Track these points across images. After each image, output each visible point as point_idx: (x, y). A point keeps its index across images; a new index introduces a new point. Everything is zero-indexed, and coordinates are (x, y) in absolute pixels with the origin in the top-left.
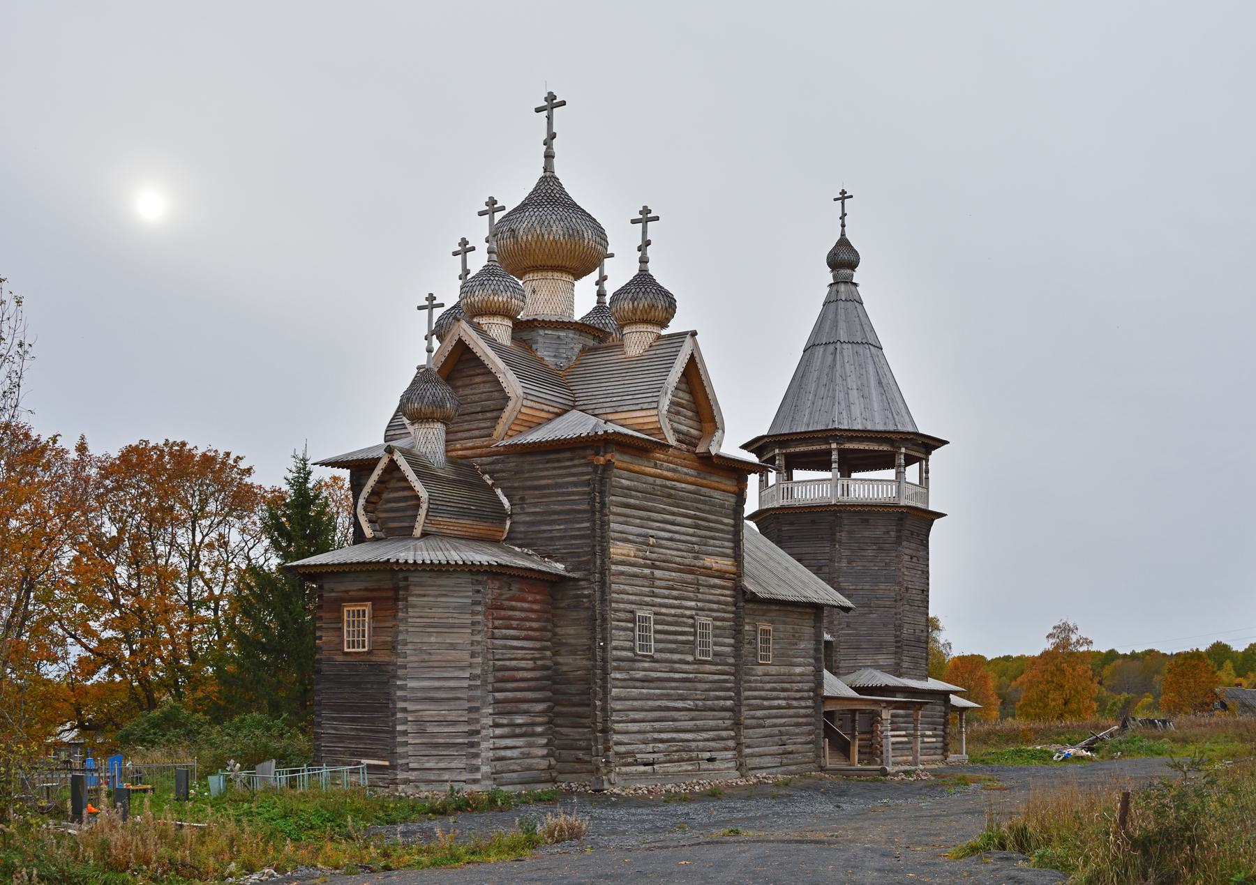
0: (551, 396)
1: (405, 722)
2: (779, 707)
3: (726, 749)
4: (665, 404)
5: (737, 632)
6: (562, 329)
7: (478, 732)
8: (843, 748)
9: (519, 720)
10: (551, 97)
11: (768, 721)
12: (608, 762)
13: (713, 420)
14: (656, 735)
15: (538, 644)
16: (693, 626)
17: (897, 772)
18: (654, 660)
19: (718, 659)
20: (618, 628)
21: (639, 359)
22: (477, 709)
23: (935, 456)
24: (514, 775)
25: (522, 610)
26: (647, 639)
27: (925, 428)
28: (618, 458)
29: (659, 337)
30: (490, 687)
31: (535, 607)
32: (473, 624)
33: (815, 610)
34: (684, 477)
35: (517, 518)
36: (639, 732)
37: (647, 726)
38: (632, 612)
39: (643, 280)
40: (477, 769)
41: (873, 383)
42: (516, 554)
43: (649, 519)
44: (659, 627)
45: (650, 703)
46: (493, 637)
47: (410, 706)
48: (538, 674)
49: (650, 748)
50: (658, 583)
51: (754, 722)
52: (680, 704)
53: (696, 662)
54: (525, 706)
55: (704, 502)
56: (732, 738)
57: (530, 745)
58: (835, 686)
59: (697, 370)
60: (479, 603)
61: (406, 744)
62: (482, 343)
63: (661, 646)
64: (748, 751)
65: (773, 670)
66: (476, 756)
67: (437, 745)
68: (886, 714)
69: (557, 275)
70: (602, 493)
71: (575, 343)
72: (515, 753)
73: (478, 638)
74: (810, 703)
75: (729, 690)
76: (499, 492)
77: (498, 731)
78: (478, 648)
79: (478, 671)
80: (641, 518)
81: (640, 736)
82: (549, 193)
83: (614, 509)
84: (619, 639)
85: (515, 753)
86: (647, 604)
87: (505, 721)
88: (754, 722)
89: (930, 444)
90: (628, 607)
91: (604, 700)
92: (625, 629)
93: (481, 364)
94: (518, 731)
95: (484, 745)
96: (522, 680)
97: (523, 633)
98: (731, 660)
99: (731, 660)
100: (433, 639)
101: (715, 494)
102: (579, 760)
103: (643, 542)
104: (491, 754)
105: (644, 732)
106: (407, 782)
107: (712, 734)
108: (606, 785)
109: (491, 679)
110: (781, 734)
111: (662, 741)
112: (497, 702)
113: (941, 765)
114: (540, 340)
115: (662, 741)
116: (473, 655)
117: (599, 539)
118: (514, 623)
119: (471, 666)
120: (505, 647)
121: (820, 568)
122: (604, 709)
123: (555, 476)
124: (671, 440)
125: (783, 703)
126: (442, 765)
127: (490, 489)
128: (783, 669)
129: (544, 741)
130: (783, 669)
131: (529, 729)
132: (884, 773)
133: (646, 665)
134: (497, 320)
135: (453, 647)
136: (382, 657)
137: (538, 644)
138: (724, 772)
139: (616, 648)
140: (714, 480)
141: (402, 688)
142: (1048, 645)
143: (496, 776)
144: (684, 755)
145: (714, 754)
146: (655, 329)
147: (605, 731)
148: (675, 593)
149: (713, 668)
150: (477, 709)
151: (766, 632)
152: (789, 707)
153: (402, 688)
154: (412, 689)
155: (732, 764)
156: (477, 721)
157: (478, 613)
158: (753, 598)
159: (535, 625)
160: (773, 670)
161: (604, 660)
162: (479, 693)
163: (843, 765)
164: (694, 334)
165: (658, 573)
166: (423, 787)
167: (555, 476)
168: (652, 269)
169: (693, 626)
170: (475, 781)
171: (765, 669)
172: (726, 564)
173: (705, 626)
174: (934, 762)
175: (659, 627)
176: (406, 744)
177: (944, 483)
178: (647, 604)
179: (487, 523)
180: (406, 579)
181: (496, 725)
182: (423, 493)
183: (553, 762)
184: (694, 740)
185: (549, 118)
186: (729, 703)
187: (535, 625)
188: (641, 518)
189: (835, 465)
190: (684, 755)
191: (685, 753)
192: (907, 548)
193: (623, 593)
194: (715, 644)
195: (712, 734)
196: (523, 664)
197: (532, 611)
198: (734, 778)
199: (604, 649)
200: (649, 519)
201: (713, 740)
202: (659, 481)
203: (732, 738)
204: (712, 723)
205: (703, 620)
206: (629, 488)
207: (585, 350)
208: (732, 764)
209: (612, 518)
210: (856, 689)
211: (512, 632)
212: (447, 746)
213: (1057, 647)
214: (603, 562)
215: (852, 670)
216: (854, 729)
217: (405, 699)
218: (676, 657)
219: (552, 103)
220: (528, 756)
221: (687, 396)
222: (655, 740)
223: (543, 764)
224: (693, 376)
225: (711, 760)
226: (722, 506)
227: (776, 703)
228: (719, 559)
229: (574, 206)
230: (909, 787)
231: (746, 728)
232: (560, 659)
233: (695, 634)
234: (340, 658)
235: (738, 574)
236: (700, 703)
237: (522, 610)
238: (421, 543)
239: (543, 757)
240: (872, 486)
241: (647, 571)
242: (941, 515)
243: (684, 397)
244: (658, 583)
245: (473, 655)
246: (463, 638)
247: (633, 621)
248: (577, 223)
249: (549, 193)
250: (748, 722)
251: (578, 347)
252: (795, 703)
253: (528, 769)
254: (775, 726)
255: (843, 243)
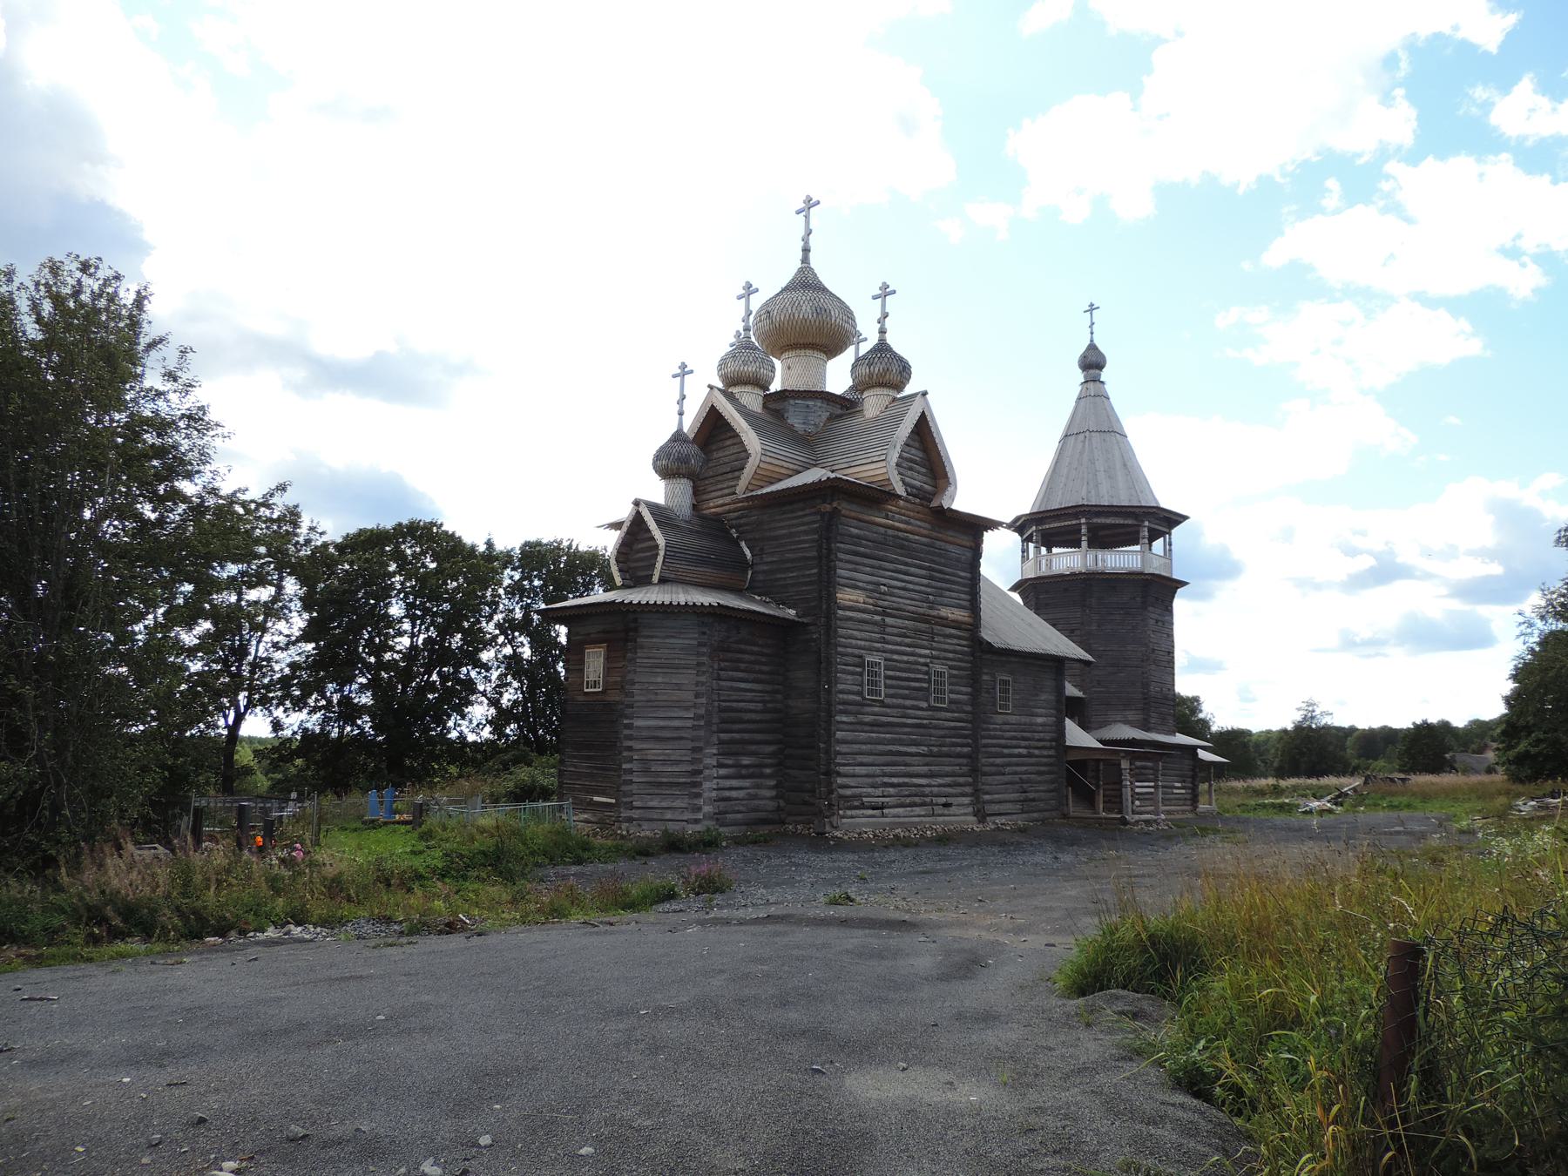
0: (787, 454)
1: (631, 760)
2: (1020, 755)
3: (963, 795)
4: (894, 457)
5: (974, 681)
6: (811, 398)
7: (700, 772)
8: (1087, 798)
9: (746, 761)
10: (885, 286)
11: (1008, 769)
12: (830, 805)
13: (945, 476)
14: (886, 780)
15: (769, 688)
16: (927, 673)
17: (1137, 822)
18: (882, 704)
19: (954, 707)
20: (844, 672)
21: (876, 419)
22: (699, 749)
23: (1176, 532)
24: (739, 816)
25: (752, 653)
26: (876, 683)
27: (1167, 502)
28: (845, 508)
29: (894, 399)
30: (714, 728)
31: (765, 651)
32: (698, 664)
33: (1057, 664)
34: (917, 529)
35: (757, 568)
36: (867, 776)
37: (877, 770)
38: (861, 657)
39: (882, 348)
40: (699, 809)
41: (1118, 465)
42: (754, 601)
43: (880, 568)
44: (890, 673)
45: (880, 747)
46: (719, 679)
47: (637, 745)
48: (768, 716)
49: (879, 791)
50: (888, 630)
51: (993, 769)
52: (913, 749)
53: (930, 708)
54: (753, 748)
55: (940, 555)
56: (969, 784)
57: (758, 787)
58: (1076, 735)
59: (929, 428)
60: (704, 645)
61: (631, 782)
62: (737, 415)
63: (892, 691)
64: (987, 797)
65: (1013, 719)
66: (698, 795)
67: (661, 784)
68: (1125, 764)
69: (808, 352)
70: (828, 539)
71: (821, 413)
72: (741, 794)
73: (703, 679)
74: (1052, 752)
75: (965, 737)
76: (743, 544)
77: (722, 772)
78: (702, 689)
79: (702, 711)
80: (872, 567)
81: (870, 780)
82: (806, 282)
83: (841, 556)
84: (846, 683)
85: (741, 794)
86: (878, 650)
87: (730, 762)
88: (993, 769)
89: (1171, 520)
90: (856, 652)
91: (828, 742)
92: (853, 673)
93: (731, 429)
94: (744, 772)
95: (707, 785)
96: (748, 721)
97: (752, 676)
98: (969, 708)
99: (969, 708)
100: (660, 680)
101: (950, 548)
102: (805, 803)
103: (873, 590)
104: (714, 794)
105: (873, 776)
106: (630, 820)
107: (948, 780)
108: (828, 828)
109: (715, 720)
110: (1022, 781)
111: (893, 785)
112: (721, 742)
113: (1190, 815)
114: (791, 409)
115: (893, 785)
116: (697, 696)
117: (827, 584)
118: (743, 666)
119: (695, 706)
120: (732, 689)
121: (1072, 631)
122: (827, 752)
123: (790, 526)
124: (900, 490)
125: (1024, 751)
126: (664, 804)
127: (736, 543)
128: (1024, 719)
129: (773, 783)
130: (1024, 719)
131: (757, 770)
132: (1124, 822)
133: (876, 709)
134: (748, 389)
135: (679, 687)
136: (614, 697)
137: (769, 688)
138: (961, 817)
139: (842, 692)
140: (950, 535)
141: (629, 727)
142: (1298, 717)
143: (719, 817)
144: (917, 800)
145: (950, 800)
146: (892, 393)
147: (828, 773)
148: (908, 640)
149: (949, 715)
150: (699, 749)
151: (1005, 683)
152: (1030, 755)
153: (629, 727)
154: (639, 727)
155: (970, 809)
156: (700, 761)
157: (703, 654)
158: (989, 648)
159: (765, 668)
160: (1013, 719)
161: (829, 703)
162: (702, 733)
163: (1087, 814)
164: (925, 394)
165: (888, 620)
166: (645, 825)
167: (790, 526)
168: (891, 340)
169: (927, 673)
170: (697, 821)
171: (1006, 718)
172: (960, 615)
173: (940, 674)
174: (1184, 812)
175: (890, 673)
176: (631, 782)
177: (1182, 551)
178: (878, 650)
179: (729, 573)
180: (635, 620)
181: (720, 766)
182: (660, 540)
183: (782, 803)
184: (929, 786)
185: (807, 217)
186: (966, 750)
187: (765, 668)
188: (872, 567)
189: (1084, 544)
190: (917, 800)
191: (917, 798)
192: (1153, 613)
193: (852, 638)
194: (951, 692)
195: (948, 780)
196: (752, 706)
197: (763, 654)
198: (971, 822)
199: (829, 691)
200: (880, 568)
201: (949, 785)
202: (890, 532)
203: (969, 784)
204: (948, 769)
205: (939, 668)
206: (858, 537)
207: (833, 418)
208: (970, 809)
209: (839, 564)
210: (1101, 741)
211: (741, 675)
212: (671, 785)
213: (1305, 719)
214: (829, 606)
215: (1104, 724)
216: (1098, 779)
217: (630, 738)
218: (908, 703)
219: (1092, 308)
220: (755, 797)
221: (920, 454)
222: (886, 785)
223: (771, 805)
224: (924, 433)
225: (946, 805)
226: (958, 560)
227: (1016, 751)
228: (955, 611)
229: (825, 290)
230: (1152, 837)
231: (985, 774)
232: (791, 703)
233: (929, 681)
234: (581, 698)
235: (973, 626)
236: (935, 749)
237: (752, 653)
238: (657, 588)
239: (771, 798)
240: (1123, 559)
241: (878, 618)
242: (1183, 584)
243: (916, 454)
244: (888, 630)
245: (697, 696)
246: (687, 678)
247: (862, 665)
248: (823, 300)
249: (806, 282)
250: (986, 769)
251: (825, 415)
252: (1036, 752)
253: (755, 810)
254: (1016, 773)
255: (1092, 347)
